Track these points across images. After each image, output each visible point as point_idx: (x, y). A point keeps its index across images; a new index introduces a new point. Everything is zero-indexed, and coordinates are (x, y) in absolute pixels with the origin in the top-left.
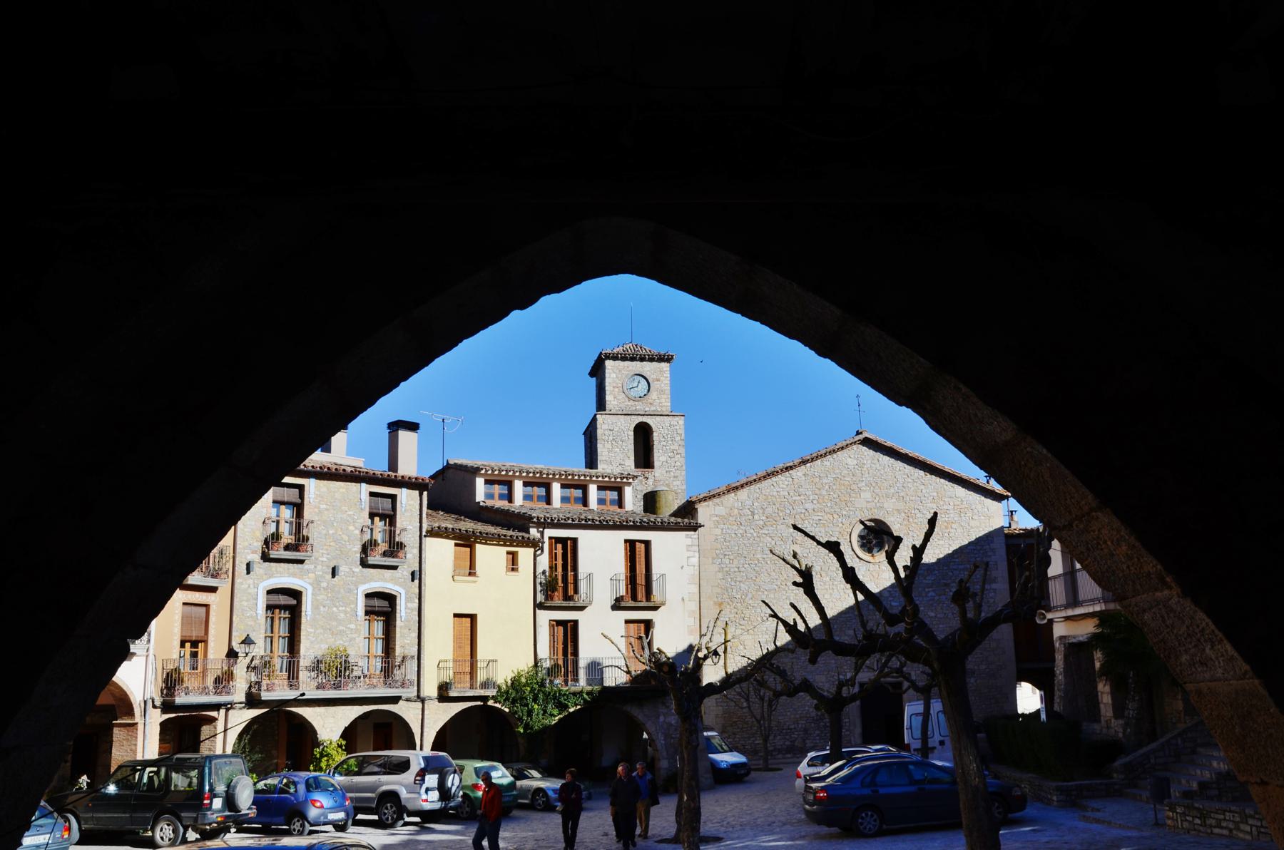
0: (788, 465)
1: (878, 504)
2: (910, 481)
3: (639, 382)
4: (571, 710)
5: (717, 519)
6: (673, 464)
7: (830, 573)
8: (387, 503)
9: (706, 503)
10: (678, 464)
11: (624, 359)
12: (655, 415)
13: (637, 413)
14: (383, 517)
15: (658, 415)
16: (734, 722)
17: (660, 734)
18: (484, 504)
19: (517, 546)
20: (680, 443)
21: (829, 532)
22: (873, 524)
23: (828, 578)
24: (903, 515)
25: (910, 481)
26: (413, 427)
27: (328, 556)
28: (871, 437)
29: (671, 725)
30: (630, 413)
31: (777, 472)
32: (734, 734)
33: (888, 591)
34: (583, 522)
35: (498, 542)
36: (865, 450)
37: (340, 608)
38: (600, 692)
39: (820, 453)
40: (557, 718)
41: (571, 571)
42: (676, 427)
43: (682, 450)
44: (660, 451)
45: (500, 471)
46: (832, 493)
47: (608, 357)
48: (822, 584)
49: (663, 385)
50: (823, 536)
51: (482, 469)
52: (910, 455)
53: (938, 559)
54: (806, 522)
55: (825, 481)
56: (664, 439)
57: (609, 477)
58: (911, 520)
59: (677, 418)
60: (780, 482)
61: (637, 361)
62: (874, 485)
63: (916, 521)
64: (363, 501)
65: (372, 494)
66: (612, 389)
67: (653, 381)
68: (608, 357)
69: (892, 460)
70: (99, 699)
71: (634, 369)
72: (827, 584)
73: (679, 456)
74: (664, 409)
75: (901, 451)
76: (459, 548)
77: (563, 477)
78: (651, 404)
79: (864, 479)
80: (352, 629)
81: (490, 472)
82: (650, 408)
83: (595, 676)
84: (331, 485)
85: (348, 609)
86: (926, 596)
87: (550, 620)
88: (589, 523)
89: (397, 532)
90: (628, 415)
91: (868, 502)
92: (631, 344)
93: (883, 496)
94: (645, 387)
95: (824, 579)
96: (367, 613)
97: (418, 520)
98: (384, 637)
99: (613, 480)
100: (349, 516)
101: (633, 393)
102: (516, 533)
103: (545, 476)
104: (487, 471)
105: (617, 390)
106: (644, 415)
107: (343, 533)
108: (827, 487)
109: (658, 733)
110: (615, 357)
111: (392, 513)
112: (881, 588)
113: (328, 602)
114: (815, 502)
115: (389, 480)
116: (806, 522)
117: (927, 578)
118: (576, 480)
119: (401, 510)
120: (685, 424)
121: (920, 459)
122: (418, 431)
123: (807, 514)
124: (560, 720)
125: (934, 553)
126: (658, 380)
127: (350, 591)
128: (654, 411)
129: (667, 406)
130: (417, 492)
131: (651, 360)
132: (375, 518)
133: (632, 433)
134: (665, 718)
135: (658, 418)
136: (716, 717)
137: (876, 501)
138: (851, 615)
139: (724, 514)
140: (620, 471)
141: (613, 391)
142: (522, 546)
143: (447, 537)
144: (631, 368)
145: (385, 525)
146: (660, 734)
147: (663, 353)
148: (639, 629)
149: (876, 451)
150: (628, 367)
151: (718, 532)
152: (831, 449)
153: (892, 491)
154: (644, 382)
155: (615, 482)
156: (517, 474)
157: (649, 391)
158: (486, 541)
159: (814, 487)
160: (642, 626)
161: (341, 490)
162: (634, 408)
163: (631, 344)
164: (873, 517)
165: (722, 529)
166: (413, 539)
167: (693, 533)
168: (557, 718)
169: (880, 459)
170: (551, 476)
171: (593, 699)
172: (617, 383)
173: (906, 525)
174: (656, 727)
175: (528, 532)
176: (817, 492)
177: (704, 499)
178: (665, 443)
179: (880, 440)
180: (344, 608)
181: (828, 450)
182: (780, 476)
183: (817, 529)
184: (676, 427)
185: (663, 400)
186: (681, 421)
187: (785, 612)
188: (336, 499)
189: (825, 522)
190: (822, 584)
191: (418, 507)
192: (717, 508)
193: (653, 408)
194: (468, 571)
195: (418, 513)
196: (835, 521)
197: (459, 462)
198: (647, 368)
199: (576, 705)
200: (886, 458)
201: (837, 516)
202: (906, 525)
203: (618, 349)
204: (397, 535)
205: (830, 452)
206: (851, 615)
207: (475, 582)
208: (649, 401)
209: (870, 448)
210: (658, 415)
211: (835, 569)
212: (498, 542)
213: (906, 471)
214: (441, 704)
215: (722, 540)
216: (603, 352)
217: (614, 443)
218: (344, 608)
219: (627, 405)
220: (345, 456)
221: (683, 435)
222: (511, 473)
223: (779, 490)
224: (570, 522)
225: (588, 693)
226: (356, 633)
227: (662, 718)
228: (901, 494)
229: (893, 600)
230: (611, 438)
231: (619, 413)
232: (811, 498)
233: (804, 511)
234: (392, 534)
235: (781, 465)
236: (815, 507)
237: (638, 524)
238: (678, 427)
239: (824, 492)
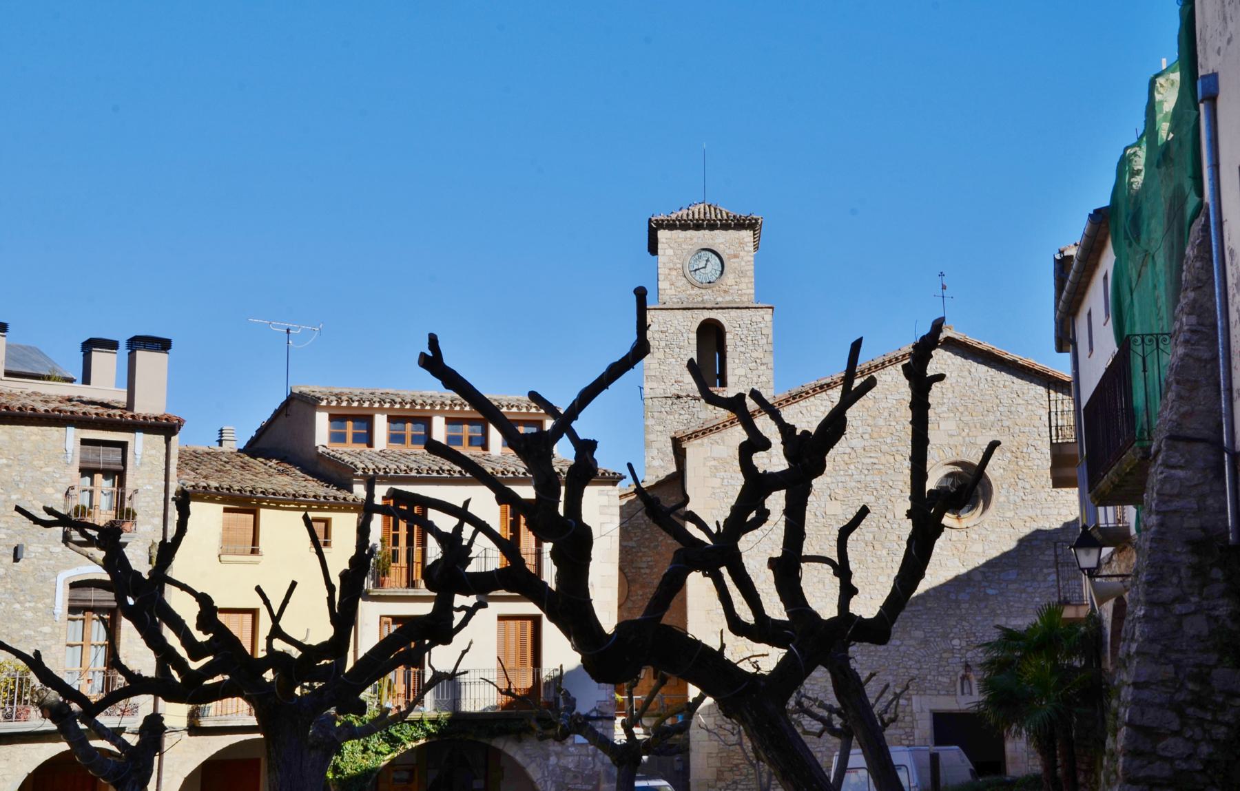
0: (823, 382)
1: (967, 439)
2: (1021, 402)
3: (708, 261)
4: (410, 746)
5: (713, 463)
6: (755, 379)
7: (887, 544)
8: (114, 455)
9: (699, 441)
10: (763, 379)
11: (685, 226)
12: (728, 308)
13: (702, 306)
14: (107, 474)
15: (732, 308)
16: (737, 765)
17: (549, 783)
18: (324, 449)
19: (330, 510)
20: (766, 347)
21: (887, 483)
22: (960, 469)
23: (885, 552)
24: (1009, 455)
25: (1021, 402)
26: (162, 345)
27: (9, 531)
28: (956, 337)
29: (569, 770)
30: (690, 306)
31: (807, 393)
32: (735, 782)
33: (981, 572)
34: (435, 474)
35: (299, 505)
36: (949, 356)
37: (27, 605)
38: (450, 720)
39: (873, 363)
40: (389, 757)
41: (418, 546)
42: (760, 325)
43: (769, 359)
44: (737, 361)
45: (350, 400)
46: (893, 423)
47: (662, 225)
48: (875, 560)
49: (743, 263)
50: (878, 487)
51: (322, 400)
52: (1020, 362)
53: (1065, 524)
54: (852, 467)
55: (883, 405)
56: (741, 343)
57: (517, 406)
58: (1021, 463)
59: (762, 312)
60: (813, 408)
61: (705, 229)
62: (961, 409)
63: (1029, 464)
64: (70, 451)
65: (84, 442)
66: (667, 271)
67: (729, 259)
68: (662, 225)
69: (992, 372)
70: (781, 656)
71: (700, 241)
72: (883, 560)
73: (764, 367)
74: (745, 299)
75: (1005, 357)
76: (231, 514)
77: (447, 408)
78: (725, 291)
79: (945, 401)
80: (45, 634)
81: (334, 404)
82: (723, 298)
83: (443, 697)
84: (17, 431)
85: (40, 605)
86: (1045, 581)
87: (381, 617)
88: (444, 475)
89: (128, 495)
90: (689, 309)
91: (951, 436)
92: (702, 206)
93: (976, 427)
94: (716, 267)
95: (879, 553)
96: (72, 610)
97: (163, 477)
98: (107, 643)
99: (524, 410)
100: (47, 473)
101: (698, 277)
102: (332, 491)
103: (418, 407)
104: (329, 403)
105: (674, 273)
106: (711, 309)
107: (34, 499)
108: (886, 414)
109: (546, 782)
110: (671, 226)
111: (122, 468)
112: (970, 568)
113: (7, 596)
114: (866, 436)
115: (110, 421)
116: (852, 467)
117: (1046, 553)
118: (467, 412)
119: (134, 464)
120: (774, 321)
121: (1036, 367)
122: (169, 351)
123: (853, 455)
124: (393, 761)
125: (1059, 514)
126: (736, 256)
127: (44, 580)
128: (729, 302)
129: (750, 294)
130: (162, 438)
131: (726, 226)
132: (96, 475)
133: (694, 336)
134: (559, 760)
135: (733, 312)
136: (708, 757)
137: (964, 434)
138: (920, 608)
139: (725, 455)
140: (676, 392)
141: (669, 274)
142: (339, 510)
143: (212, 500)
144: (695, 240)
145: (114, 486)
146: (549, 783)
147: (744, 215)
148: (523, 629)
149: (966, 358)
150: (691, 239)
151: (716, 482)
152: (891, 356)
153: (991, 417)
154: (714, 260)
155: (528, 413)
156: (377, 405)
157: (722, 272)
158: (278, 504)
159: (865, 414)
160: (529, 623)
161: (33, 438)
162: (700, 299)
163: (702, 206)
164: (959, 459)
165: (723, 479)
166: (153, 504)
167: (610, 488)
168: (389, 757)
169: (973, 370)
170: (428, 408)
171: (441, 731)
172: (675, 264)
173: (1012, 471)
174: (543, 773)
175: (351, 491)
176: (870, 421)
177: (695, 435)
178: (743, 349)
179: (972, 340)
180: (32, 604)
181: (887, 358)
182: (812, 399)
183: (869, 478)
184: (760, 325)
185: (743, 286)
186: (768, 315)
187: (817, 601)
188: (24, 450)
189: (882, 467)
190: (875, 560)
191: (163, 459)
192: (716, 447)
193: (728, 298)
194: (250, 548)
195: (164, 467)
196: (897, 466)
197: (305, 389)
198: (720, 239)
199: (416, 739)
200: (983, 368)
201: (902, 458)
202: (1012, 471)
203: (680, 213)
204: (126, 499)
205: (890, 361)
206: (920, 608)
207: (257, 563)
208: (724, 287)
209: (956, 354)
210: (732, 308)
211: (895, 538)
212: (299, 505)
213: (1015, 387)
214: (193, 738)
215: (722, 495)
216: (653, 219)
217: (667, 350)
218: (32, 604)
219: (690, 295)
220: (114, 389)
221: (771, 337)
222: (366, 405)
223: (810, 419)
224: (414, 473)
225: (432, 722)
226: (52, 638)
227: (553, 760)
228: (1006, 423)
229: (989, 586)
230: (663, 343)
231: (675, 307)
232: (860, 431)
233: (848, 450)
234: (121, 498)
235: (813, 383)
236: (867, 444)
237: (521, 476)
238: (762, 325)
239: (881, 422)
